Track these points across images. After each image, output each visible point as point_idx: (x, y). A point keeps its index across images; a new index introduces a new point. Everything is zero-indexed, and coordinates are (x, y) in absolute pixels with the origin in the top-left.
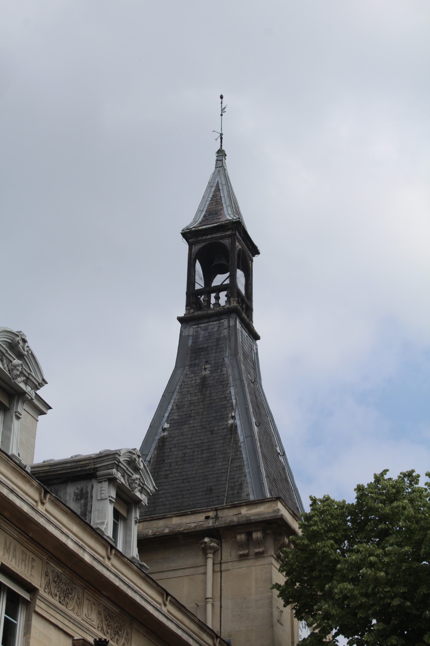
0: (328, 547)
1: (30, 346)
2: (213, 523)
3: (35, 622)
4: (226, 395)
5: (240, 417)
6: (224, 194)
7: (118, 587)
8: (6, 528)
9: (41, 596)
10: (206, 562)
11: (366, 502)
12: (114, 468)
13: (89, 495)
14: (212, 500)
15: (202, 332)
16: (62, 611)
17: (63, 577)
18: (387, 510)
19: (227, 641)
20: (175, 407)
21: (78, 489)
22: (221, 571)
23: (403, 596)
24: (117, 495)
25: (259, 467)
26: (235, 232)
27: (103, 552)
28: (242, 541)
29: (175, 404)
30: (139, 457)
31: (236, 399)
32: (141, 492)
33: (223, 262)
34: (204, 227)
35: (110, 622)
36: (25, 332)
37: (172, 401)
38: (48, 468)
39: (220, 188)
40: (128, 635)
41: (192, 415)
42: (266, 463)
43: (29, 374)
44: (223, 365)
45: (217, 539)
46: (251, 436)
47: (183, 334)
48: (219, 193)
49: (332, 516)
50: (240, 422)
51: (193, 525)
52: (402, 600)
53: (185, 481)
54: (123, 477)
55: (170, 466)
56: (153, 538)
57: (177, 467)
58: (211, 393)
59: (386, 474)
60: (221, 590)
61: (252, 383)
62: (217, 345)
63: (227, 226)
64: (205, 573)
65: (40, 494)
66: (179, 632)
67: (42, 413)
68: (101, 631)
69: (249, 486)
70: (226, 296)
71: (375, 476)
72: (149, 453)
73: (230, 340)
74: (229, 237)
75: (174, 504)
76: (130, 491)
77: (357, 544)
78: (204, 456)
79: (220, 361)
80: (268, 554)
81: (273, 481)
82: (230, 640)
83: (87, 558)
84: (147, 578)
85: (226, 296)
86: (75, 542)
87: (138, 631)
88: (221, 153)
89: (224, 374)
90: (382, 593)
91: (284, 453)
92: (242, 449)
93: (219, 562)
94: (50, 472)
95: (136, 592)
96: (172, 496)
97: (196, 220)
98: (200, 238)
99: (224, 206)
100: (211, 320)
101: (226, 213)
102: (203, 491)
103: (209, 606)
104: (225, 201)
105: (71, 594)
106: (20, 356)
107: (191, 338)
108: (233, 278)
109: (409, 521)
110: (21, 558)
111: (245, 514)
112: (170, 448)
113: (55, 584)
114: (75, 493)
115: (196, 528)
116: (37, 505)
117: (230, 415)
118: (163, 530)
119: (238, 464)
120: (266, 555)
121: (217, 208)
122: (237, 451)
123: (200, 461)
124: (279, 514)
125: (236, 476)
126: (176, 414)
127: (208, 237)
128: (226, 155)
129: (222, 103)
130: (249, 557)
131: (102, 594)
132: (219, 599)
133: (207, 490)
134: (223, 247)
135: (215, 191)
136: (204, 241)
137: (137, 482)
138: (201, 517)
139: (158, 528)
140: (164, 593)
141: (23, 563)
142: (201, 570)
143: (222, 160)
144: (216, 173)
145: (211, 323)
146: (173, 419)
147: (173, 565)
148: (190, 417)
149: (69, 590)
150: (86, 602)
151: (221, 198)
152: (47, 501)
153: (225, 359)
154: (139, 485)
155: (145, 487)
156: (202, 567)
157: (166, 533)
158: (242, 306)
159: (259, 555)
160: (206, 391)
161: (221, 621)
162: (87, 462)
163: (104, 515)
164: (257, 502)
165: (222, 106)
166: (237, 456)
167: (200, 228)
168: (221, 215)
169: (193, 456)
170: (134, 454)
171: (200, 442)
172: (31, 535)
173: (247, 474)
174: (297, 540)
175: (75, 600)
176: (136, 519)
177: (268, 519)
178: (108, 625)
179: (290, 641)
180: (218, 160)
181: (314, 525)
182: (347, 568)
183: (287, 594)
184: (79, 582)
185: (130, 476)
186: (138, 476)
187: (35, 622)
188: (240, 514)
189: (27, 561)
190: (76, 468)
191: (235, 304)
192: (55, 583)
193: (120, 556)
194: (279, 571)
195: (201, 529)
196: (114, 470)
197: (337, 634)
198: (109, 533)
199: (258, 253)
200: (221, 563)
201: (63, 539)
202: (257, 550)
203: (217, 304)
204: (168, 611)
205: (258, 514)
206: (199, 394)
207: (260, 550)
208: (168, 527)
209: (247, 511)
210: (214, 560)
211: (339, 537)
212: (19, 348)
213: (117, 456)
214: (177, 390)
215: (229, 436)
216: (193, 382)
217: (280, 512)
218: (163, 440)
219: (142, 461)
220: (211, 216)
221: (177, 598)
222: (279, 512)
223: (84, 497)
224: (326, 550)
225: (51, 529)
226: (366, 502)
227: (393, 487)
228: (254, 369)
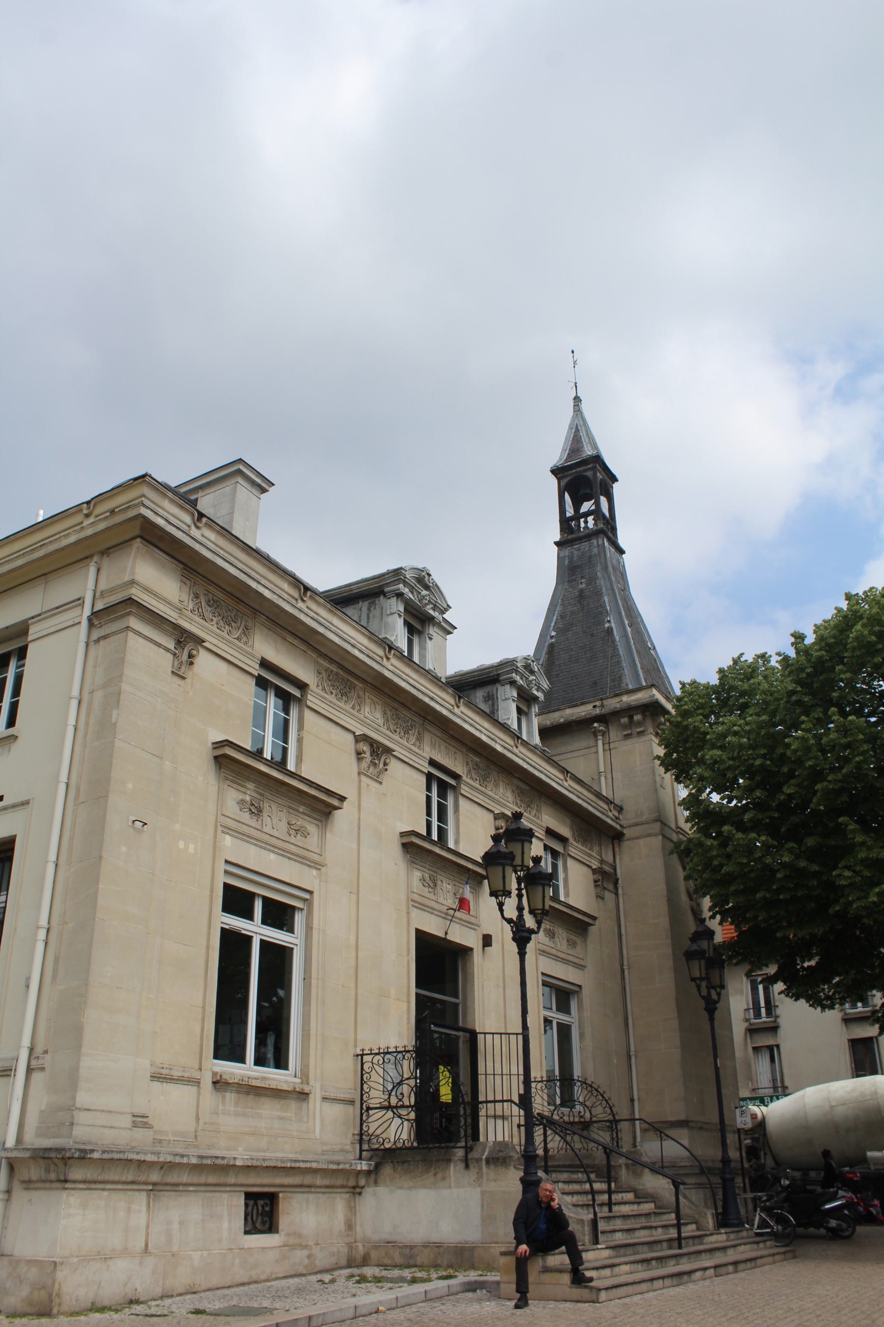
6: (583, 434)
14: (597, 691)
18: (746, 686)
23: (764, 756)
25: (634, 661)
36: (429, 567)
37: (556, 613)
44: (596, 578)
46: (626, 635)
48: (578, 434)
51: (583, 714)
54: (412, 593)
62: (590, 562)
64: (597, 752)
66: (580, 801)
67: (264, 491)
81: (647, 672)
83: (499, 748)
84: (549, 760)
88: (577, 399)
92: (619, 647)
95: (541, 772)
103: (603, 779)
104: (585, 440)
106: (427, 588)
108: (597, 504)
134: (586, 478)
136: (570, 475)
138: (589, 707)
142: (593, 750)
147: (570, 748)
150: (501, 784)
152: (461, 705)
159: (640, 734)
163: (509, 712)
166: (615, 653)
175: (241, 630)
183: (667, 763)
186: (534, 678)
193: (525, 744)
196: (514, 675)
197: (710, 793)
199: (617, 480)
201: (477, 734)
202: (638, 730)
203: (586, 527)
207: (641, 729)
218: (552, 646)
223: (491, 699)
225: (466, 726)
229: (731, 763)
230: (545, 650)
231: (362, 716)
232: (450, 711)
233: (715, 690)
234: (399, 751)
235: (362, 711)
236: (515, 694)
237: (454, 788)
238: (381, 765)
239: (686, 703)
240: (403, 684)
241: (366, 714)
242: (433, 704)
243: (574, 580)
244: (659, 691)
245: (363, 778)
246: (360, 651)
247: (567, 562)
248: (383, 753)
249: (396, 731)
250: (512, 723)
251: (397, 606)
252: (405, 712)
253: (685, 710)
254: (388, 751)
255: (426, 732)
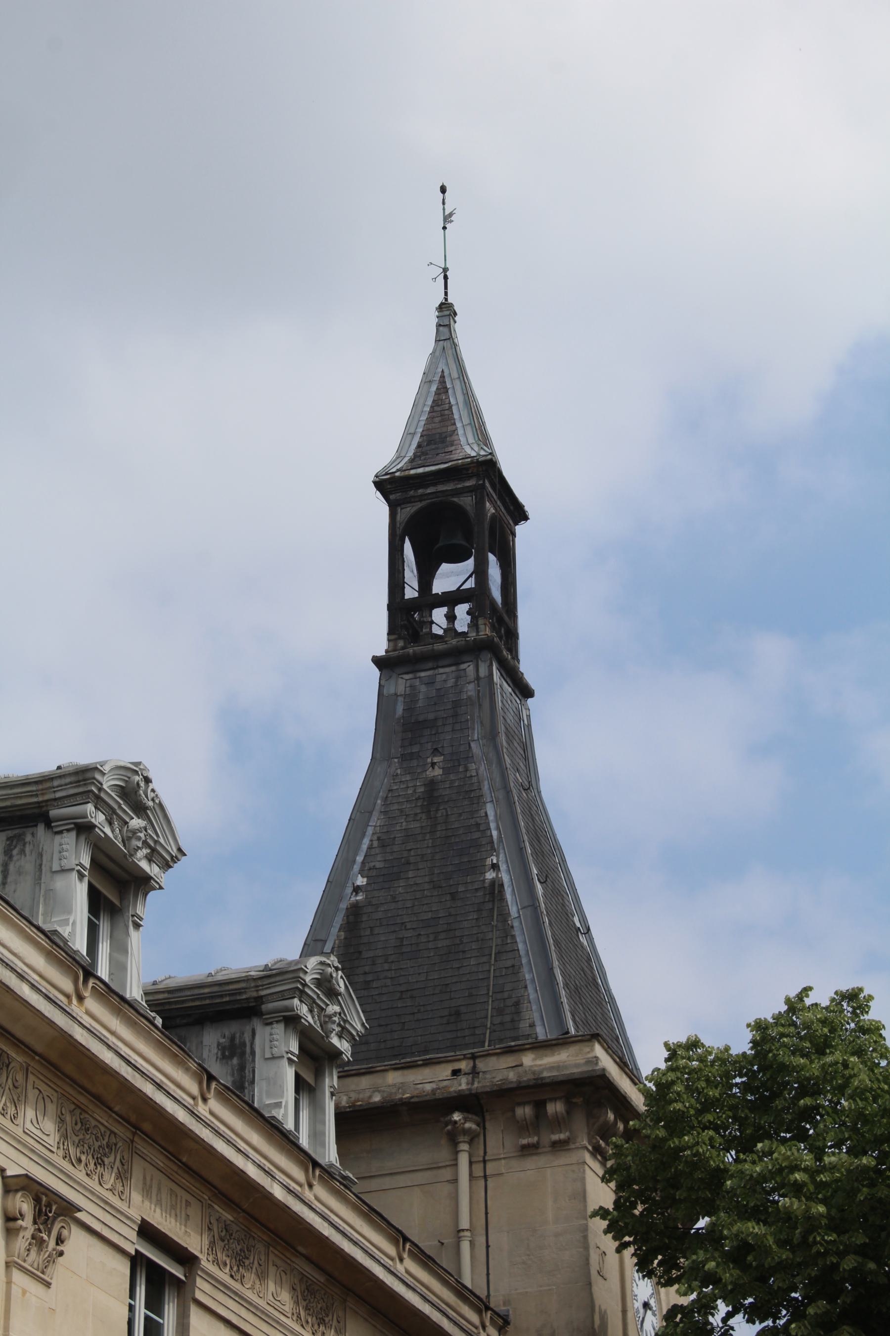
0: (705, 1144)
1: (156, 789)
2: (468, 1084)
3: (198, 1321)
4: (478, 819)
5: (508, 866)
6: (456, 399)
7: (327, 1238)
8: (145, 1151)
9: (203, 1270)
10: (456, 1159)
11: (774, 1054)
12: (88, 802)
13: (248, 1050)
15: (423, 689)
16: (236, 1294)
17: (235, 1228)
18: (815, 1068)
19: (501, 1314)
20: (375, 844)
21: (224, 1037)
22: (485, 1177)
23: (862, 1251)
24: (301, 1048)
25: (551, 969)
26: (484, 481)
27: (298, 1174)
28: (525, 1119)
29: (375, 837)
30: (337, 969)
31: (498, 828)
32: (340, 1037)
33: (460, 540)
34: (421, 470)
35: (310, 1301)
36: (147, 763)
37: (370, 831)
38: (166, 995)
39: (449, 386)
40: (339, 1322)
41: (412, 860)
42: (561, 958)
43: (156, 842)
44: (469, 757)
45: (476, 1114)
46: (533, 905)
47: (385, 692)
48: (444, 403)
49: (708, 1081)
50: (508, 877)
51: (428, 1087)
52: (860, 1259)
53: (404, 996)
54: (110, 823)
55: (374, 964)
56: (350, 1112)
57: (386, 966)
58: (447, 815)
59: (807, 996)
60: (487, 1213)
61: (525, 790)
62: (455, 715)
63: (467, 469)
64: (455, 1181)
65: (200, 1083)
66: (426, 1309)
68: (213, 1262)
69: (534, 1007)
70: (468, 613)
71: (788, 1001)
72: (330, 937)
73: (480, 705)
74: (471, 491)
75: (384, 1041)
76: (323, 1037)
77: (762, 1142)
78: (440, 944)
79: (462, 748)
80: (577, 1145)
82: (508, 1311)
83: (278, 1192)
85: (468, 613)
86: (259, 1166)
87: (356, 1313)
88: (446, 310)
89: (471, 776)
90: (822, 1245)
91: (589, 929)
92: (517, 932)
93: (481, 1159)
94: (169, 1003)
95: (355, 1243)
96: (380, 1026)
97: (403, 455)
98: (412, 493)
99: (459, 425)
100: (440, 663)
101: (463, 440)
102: (442, 1017)
103: (465, 1246)
104: (460, 414)
105: (248, 1258)
106: (140, 809)
107: (401, 699)
108: (480, 572)
109: (861, 1100)
110: (169, 1204)
111: (532, 1066)
112: (371, 928)
113: (222, 1244)
114: (219, 1044)
115: (435, 1094)
116: (196, 1105)
117: (489, 862)
118: (370, 1097)
119: (509, 963)
120: (573, 1146)
121: (444, 430)
122: (506, 937)
123: (432, 954)
124: (598, 1068)
125: (508, 987)
126: (379, 858)
127: (429, 491)
128: (455, 314)
129: (444, 203)
130: (540, 1150)
131: (297, 1251)
132: (484, 1232)
133: (450, 1015)
134: (460, 511)
135: (438, 393)
136: (421, 498)
137: (336, 1019)
138: (444, 1072)
139: (359, 1093)
140: (399, 1237)
141: (173, 1212)
142: (447, 1174)
143: (449, 326)
144: (437, 353)
145: (441, 670)
146: (374, 868)
148: (408, 863)
149: (104, 1149)
150: (272, 1270)
151: (451, 407)
152: (211, 1095)
153: (473, 745)
154: (339, 1025)
155: (347, 1026)
156: (448, 1169)
157: (375, 1103)
158: (498, 621)
159: (559, 1146)
160: (437, 810)
161: (488, 1274)
162: (243, 985)
164: (554, 1042)
165: (444, 209)
166: (507, 947)
167: (413, 472)
168: (452, 445)
169: (417, 944)
170: (329, 965)
171: (430, 915)
172: (184, 1160)
173: (528, 982)
174: (644, 1128)
175: (115, 1170)
176: (332, 1090)
177: (576, 1076)
178: (307, 1309)
179: (620, 1308)
180: (440, 325)
181: (676, 1101)
182: (744, 1187)
183: (619, 1223)
184: (259, 1234)
185: (322, 1009)
186: (337, 1009)
187: (198, 1321)
188: (521, 1065)
189: (179, 1206)
190: (221, 996)
191: (488, 632)
192: (223, 1241)
194: (602, 1181)
195: (445, 1095)
196: (296, 1001)
197: (729, 1315)
198: (80, 945)
199: (525, 518)
200: (485, 1161)
202: (555, 1137)
204: (407, 1272)
205: (558, 1068)
206: (424, 816)
207: (562, 1136)
208: (379, 1091)
209: (534, 1059)
210: (470, 1156)
211: (722, 1122)
212: (140, 795)
213: (302, 975)
214: (378, 807)
215: (490, 906)
216: (410, 791)
217: (600, 1063)
218: (355, 911)
219: (342, 977)
220: (433, 447)
221: (389, 1219)
222: (597, 1064)
223: (238, 1053)
224: (701, 1150)
225: (220, 1146)
226: (774, 1054)
227: (824, 1022)
228: (526, 759)
229: (785, 1255)
230: (339, 920)
231: (19, 1131)
232: (192, 1113)
233: (741, 1064)
234: (90, 1212)
235: (20, 1121)
236: (294, 1047)
237: (179, 1285)
238: (52, 1243)
239: (679, 1097)
240: (108, 1057)
241: (28, 1125)
242: (160, 1098)
243: (411, 756)
244: (608, 1049)
245: (18, 1277)
246: (33, 986)
247: (400, 709)
248: (57, 1215)
249: (79, 1161)
250: (72, 933)
251: (78, 856)
252: (100, 1115)
253: (676, 1111)
254: (68, 1210)
255: (136, 1159)
